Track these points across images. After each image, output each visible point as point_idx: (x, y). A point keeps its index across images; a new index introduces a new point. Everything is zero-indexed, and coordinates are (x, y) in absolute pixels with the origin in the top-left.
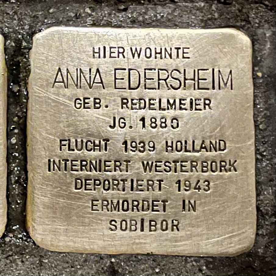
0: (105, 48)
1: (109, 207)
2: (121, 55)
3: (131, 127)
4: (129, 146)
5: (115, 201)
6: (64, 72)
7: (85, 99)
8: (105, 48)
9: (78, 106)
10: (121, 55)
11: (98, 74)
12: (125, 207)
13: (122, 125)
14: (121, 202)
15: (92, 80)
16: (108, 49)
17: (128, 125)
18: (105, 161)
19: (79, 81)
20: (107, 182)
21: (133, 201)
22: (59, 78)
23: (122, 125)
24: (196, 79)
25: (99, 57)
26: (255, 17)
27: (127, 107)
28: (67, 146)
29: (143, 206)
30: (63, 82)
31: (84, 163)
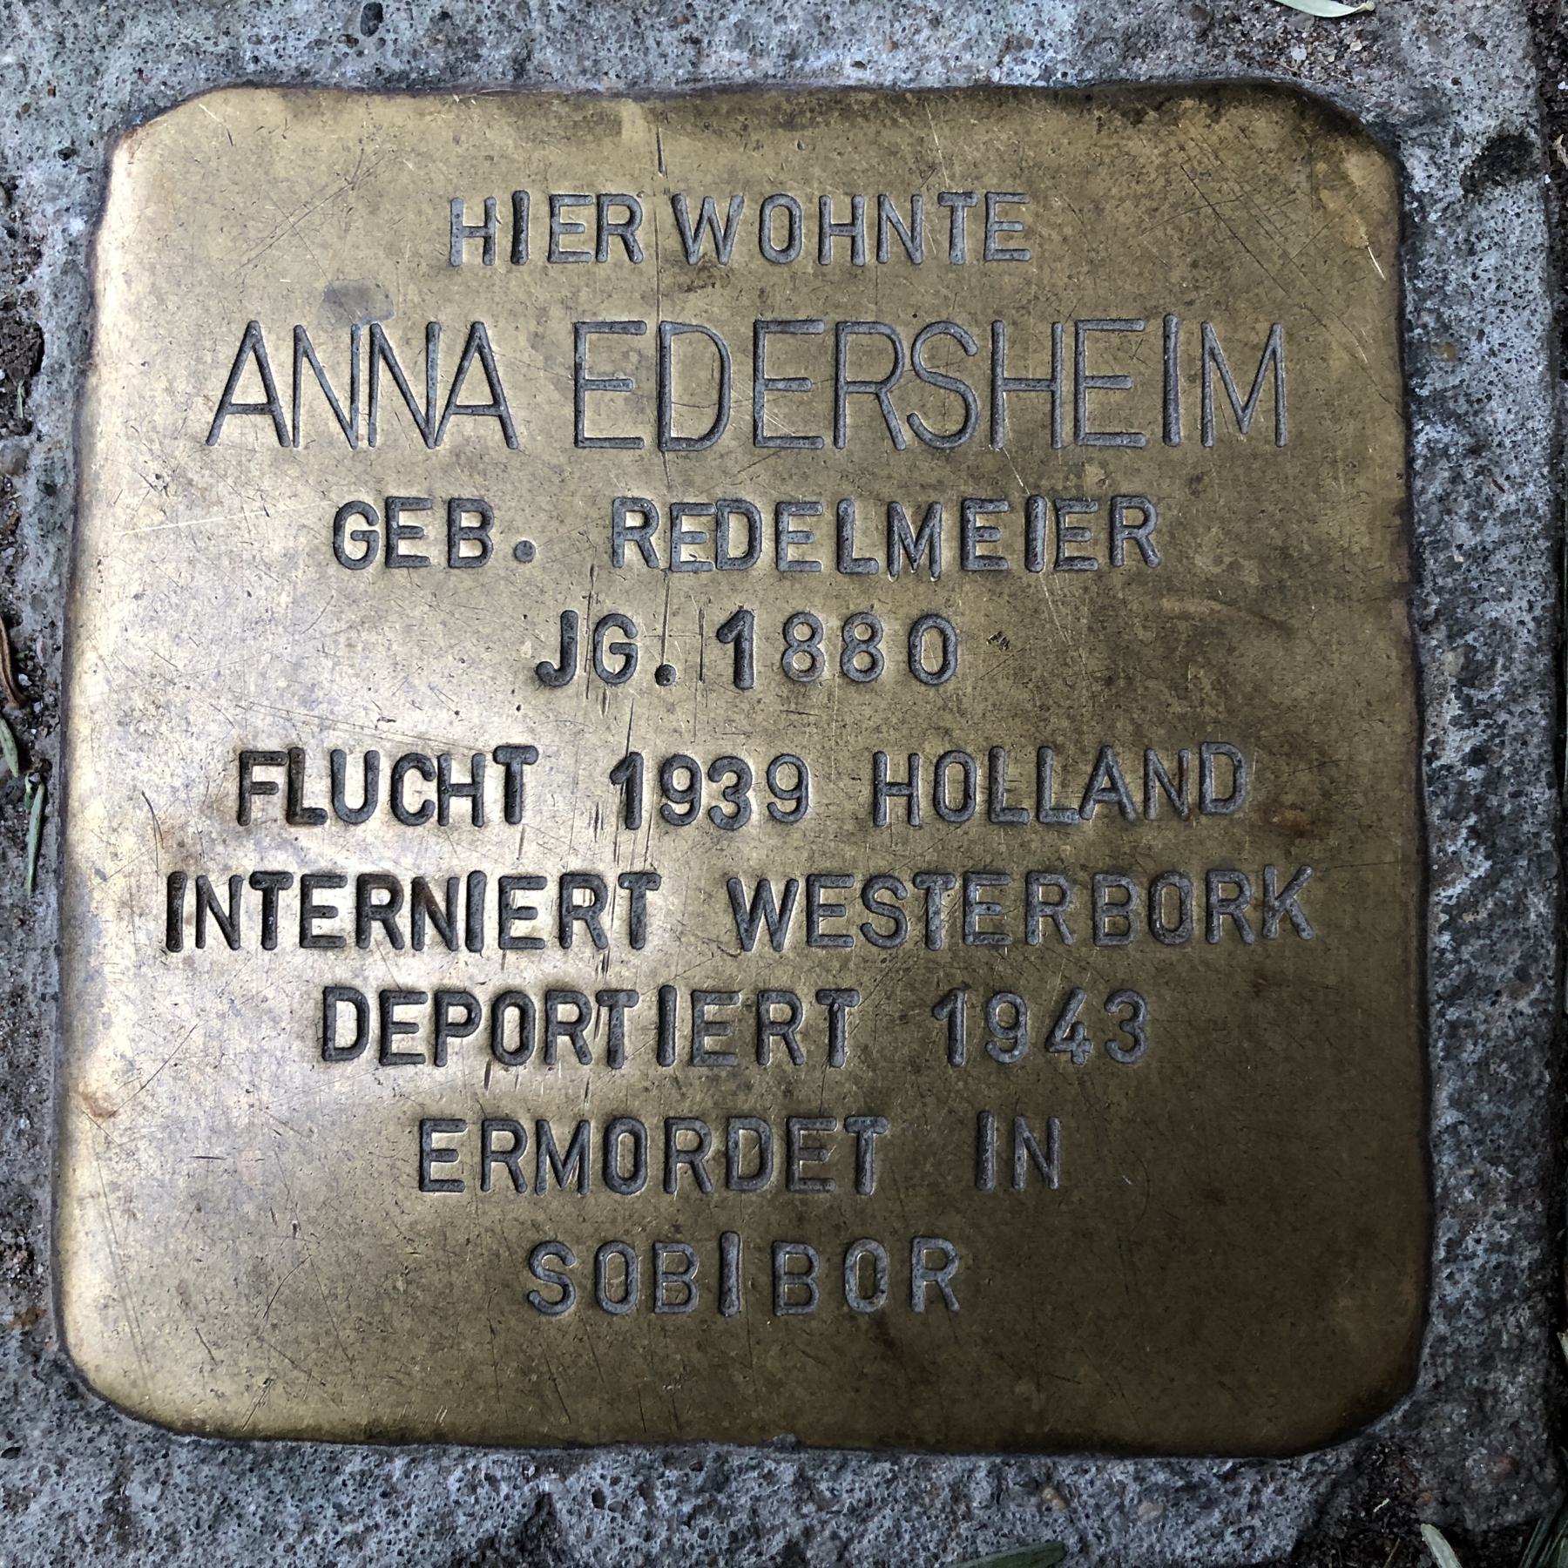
0: (517, 202)
1: (524, 1160)
2: (614, 245)
3: (662, 675)
4: (648, 797)
5: (559, 1133)
6: (279, 358)
7: (390, 505)
8: (517, 202)
9: (354, 550)
10: (614, 245)
11: (475, 363)
12: (621, 1162)
13: (613, 663)
14: (593, 1136)
15: (441, 403)
16: (536, 207)
17: (644, 669)
18: (505, 884)
19: (363, 376)
20: (511, 1015)
21: (668, 1125)
22: (249, 390)
23: (613, 663)
24: (1065, 387)
25: (477, 817)
26: (716, 1508)
27: (581, 1054)
28: (279, 799)
29: (727, 1157)
30: (268, 407)
31: (380, 897)
